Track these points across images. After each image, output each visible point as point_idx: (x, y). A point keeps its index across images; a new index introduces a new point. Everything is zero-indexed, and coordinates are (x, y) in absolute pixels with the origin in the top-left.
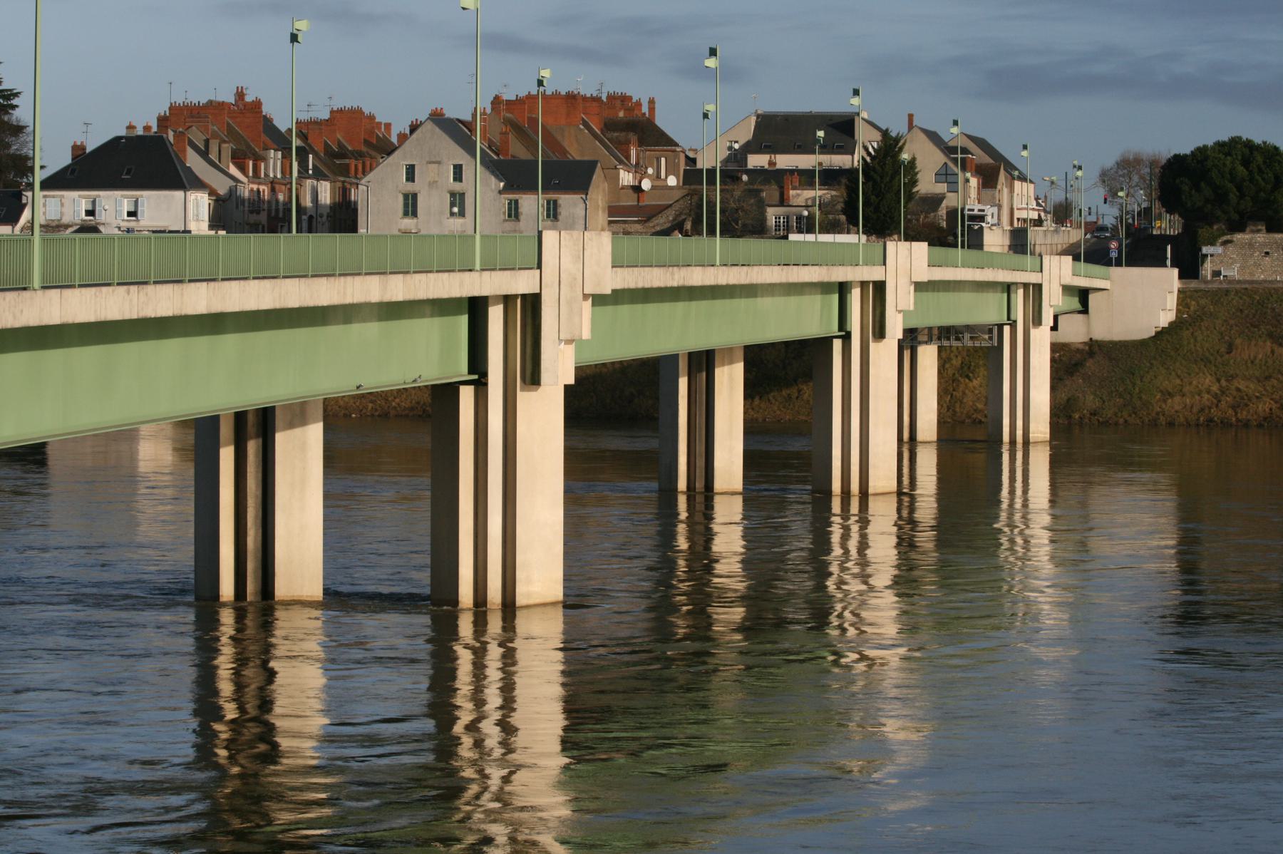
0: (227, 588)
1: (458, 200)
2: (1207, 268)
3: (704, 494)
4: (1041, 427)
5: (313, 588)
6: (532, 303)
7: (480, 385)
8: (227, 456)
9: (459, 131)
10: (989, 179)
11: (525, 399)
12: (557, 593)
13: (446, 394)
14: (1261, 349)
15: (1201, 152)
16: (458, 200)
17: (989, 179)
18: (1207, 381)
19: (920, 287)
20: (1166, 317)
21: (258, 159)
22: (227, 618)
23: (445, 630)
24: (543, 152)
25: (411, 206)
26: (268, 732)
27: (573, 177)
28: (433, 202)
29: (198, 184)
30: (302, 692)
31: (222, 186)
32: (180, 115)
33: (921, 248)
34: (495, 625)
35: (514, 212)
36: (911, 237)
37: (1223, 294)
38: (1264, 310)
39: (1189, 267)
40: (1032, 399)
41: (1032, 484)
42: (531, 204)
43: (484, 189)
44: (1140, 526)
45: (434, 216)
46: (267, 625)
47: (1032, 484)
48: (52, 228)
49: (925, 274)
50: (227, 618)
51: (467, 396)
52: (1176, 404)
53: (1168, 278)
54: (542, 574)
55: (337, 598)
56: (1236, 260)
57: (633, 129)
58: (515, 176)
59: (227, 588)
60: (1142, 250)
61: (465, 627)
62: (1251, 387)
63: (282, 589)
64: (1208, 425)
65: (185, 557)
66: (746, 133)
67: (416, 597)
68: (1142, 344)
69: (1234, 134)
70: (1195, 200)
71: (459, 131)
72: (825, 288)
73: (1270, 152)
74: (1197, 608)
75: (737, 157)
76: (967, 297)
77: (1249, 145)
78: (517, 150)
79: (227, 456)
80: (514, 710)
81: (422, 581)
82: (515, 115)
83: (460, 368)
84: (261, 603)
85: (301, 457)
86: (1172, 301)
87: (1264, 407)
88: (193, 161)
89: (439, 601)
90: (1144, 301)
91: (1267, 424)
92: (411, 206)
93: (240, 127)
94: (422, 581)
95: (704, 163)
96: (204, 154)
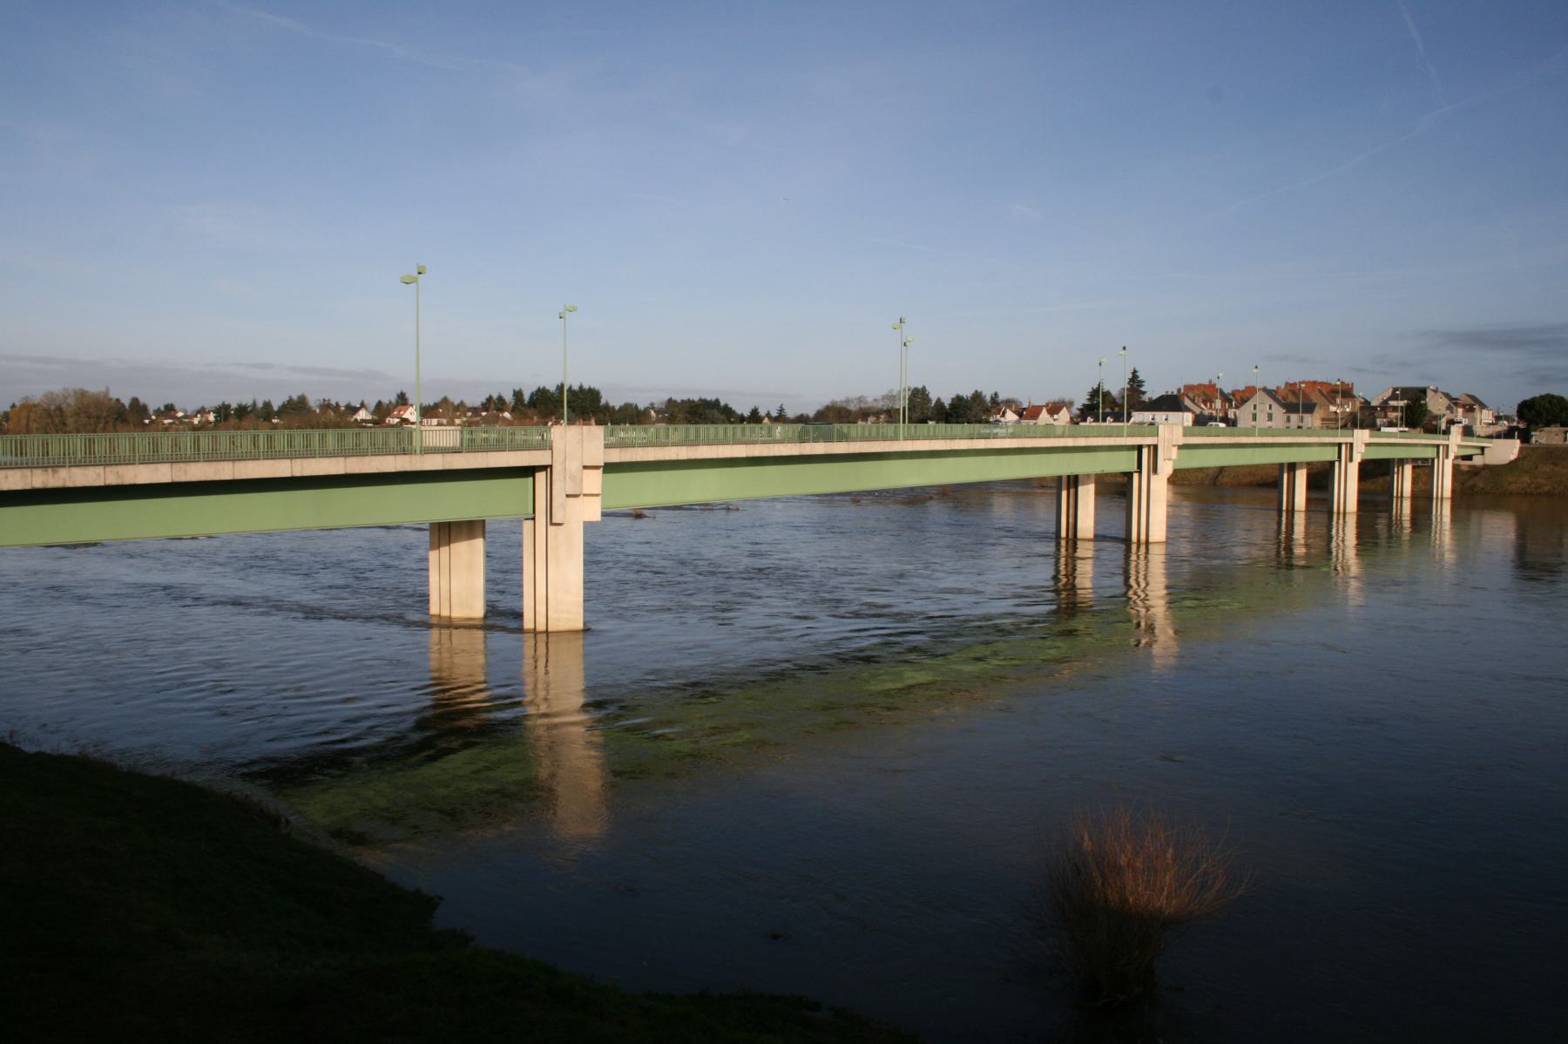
0: (1063, 534)
3: (1291, 511)
4: (1448, 493)
6: (1156, 447)
7: (1140, 473)
8: (1064, 493)
9: (1271, 393)
10: (1469, 409)
11: (1153, 477)
12: (1163, 539)
14: (1548, 468)
16: (1270, 417)
17: (1469, 409)
19: (1367, 445)
20: (1513, 457)
23: (1128, 550)
24: (1296, 400)
25: (1254, 418)
26: (1074, 587)
27: (1309, 408)
28: (1262, 417)
30: (1085, 575)
31: (1198, 411)
32: (1189, 388)
33: (1367, 432)
34: (1143, 548)
35: (1288, 420)
36: (1362, 427)
37: (1535, 449)
39: (1525, 437)
40: (1444, 483)
41: (1443, 512)
43: (1278, 411)
44: (1499, 531)
45: (1262, 422)
46: (1075, 548)
47: (1443, 512)
48: (1141, 424)
49: (600, 456)
51: (1136, 476)
52: (1513, 487)
53: (1517, 443)
54: (1158, 532)
55: (1098, 538)
56: (1546, 437)
59: (1063, 534)
60: (1509, 434)
61: (1134, 548)
62: (1543, 481)
63: (1080, 535)
64: (1525, 494)
65: (1053, 529)
66: (1389, 393)
67: (1120, 539)
71: (1271, 393)
73: (1561, 399)
75: (1385, 402)
76: (1419, 449)
77: (1553, 397)
78: (1292, 399)
79: (1064, 493)
80: (267, 405)
82: (1292, 388)
84: (1073, 541)
85: (1087, 493)
86: (1516, 451)
87: (1546, 488)
88: (1187, 402)
89: (1127, 541)
90: (1508, 451)
92: (1254, 418)
93: (1207, 393)
94: (1122, 535)
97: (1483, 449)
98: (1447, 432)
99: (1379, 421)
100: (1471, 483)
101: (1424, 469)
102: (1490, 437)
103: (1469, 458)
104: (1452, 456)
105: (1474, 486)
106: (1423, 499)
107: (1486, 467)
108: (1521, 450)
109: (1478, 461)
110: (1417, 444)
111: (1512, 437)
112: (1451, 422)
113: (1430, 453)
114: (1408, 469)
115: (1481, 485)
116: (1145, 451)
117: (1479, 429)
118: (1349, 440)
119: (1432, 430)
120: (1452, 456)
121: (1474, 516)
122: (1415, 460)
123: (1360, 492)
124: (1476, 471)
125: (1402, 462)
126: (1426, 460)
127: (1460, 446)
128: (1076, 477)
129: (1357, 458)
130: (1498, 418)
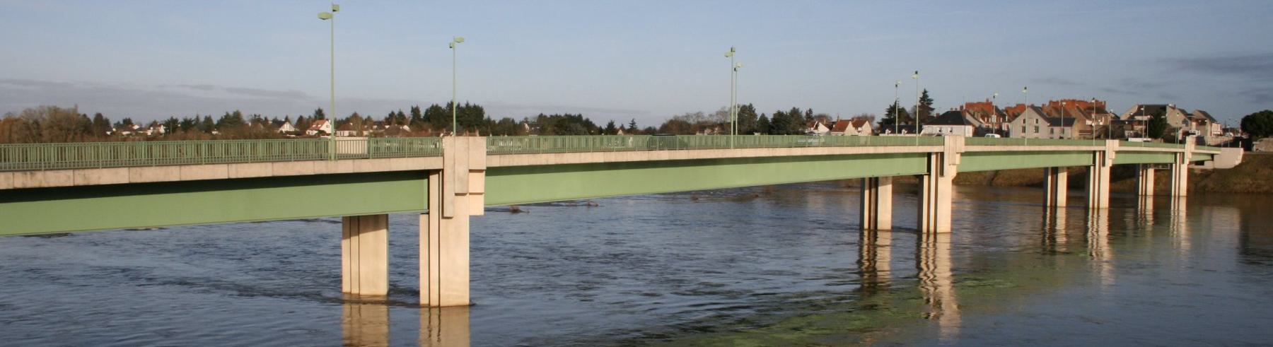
0: (866, 226)
1: (1037, 129)
2: (1254, 148)
3: (1054, 207)
4: (1183, 192)
5: (889, 227)
6: (942, 154)
8: (867, 192)
10: (1201, 123)
12: (949, 230)
13: (920, 177)
14: (1266, 171)
15: (1254, 115)
16: (1037, 129)
17: (1201, 123)
18: (1249, 181)
19: (1117, 152)
20: (1238, 162)
21: (988, 117)
22: (866, 233)
23: (920, 239)
25: (1024, 130)
26: (875, 269)
27: (1069, 122)
29: (969, 123)
30: (884, 260)
31: (977, 124)
32: (970, 105)
33: (1117, 142)
34: (932, 238)
35: (1052, 132)
36: (1113, 138)
38: (1272, 161)
39: (1247, 146)
40: (1181, 184)
41: (1180, 208)
42: (1057, 129)
45: (1030, 134)
46: (876, 238)
47: (1180, 208)
50: (866, 233)
51: (926, 178)
52: (1238, 187)
53: (1241, 151)
54: (945, 224)
55: (895, 229)
57: (1101, 109)
58: (1054, 122)
59: (866, 226)
60: (1234, 144)
63: (879, 227)
66: (1135, 110)
67: (913, 230)
68: (1229, 170)
69: (508, 116)
70: (1256, 127)
72: (1089, 152)
74: (1251, 251)
75: (1132, 117)
76: (1160, 156)
78: (1055, 115)
79: (867, 192)
80: (208, 119)
81: (915, 226)
82: (1055, 105)
83: (925, 171)
84: (874, 231)
85: (886, 192)
86: (1240, 157)
88: (968, 117)
89: (918, 231)
91: (1267, 193)
92: (1024, 130)
93: (985, 109)
94: (915, 226)
95: (1123, 118)
96: (973, 116)
97: (1212, 155)
98: (1183, 142)
99: (1126, 133)
100: (1203, 183)
101: (1164, 173)
102: (1219, 146)
103: (1202, 163)
104: (1187, 161)
105: (1205, 186)
106: (1163, 197)
107: (1215, 171)
108: (1244, 156)
109: (1208, 165)
110: (1158, 151)
111: (1237, 146)
112: (1187, 134)
113: (1168, 159)
114: (1151, 172)
115: (1211, 185)
116: (933, 158)
117: (1209, 139)
118: (1102, 148)
119: (1171, 140)
120: (1187, 161)
121: (1206, 211)
122: (1156, 165)
123: (1111, 191)
124: (1207, 174)
125: (1146, 166)
126: (1166, 165)
127: (1193, 154)
128: (877, 179)
129: (1109, 163)
130: (1225, 130)
